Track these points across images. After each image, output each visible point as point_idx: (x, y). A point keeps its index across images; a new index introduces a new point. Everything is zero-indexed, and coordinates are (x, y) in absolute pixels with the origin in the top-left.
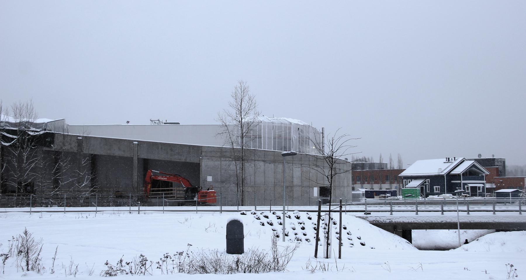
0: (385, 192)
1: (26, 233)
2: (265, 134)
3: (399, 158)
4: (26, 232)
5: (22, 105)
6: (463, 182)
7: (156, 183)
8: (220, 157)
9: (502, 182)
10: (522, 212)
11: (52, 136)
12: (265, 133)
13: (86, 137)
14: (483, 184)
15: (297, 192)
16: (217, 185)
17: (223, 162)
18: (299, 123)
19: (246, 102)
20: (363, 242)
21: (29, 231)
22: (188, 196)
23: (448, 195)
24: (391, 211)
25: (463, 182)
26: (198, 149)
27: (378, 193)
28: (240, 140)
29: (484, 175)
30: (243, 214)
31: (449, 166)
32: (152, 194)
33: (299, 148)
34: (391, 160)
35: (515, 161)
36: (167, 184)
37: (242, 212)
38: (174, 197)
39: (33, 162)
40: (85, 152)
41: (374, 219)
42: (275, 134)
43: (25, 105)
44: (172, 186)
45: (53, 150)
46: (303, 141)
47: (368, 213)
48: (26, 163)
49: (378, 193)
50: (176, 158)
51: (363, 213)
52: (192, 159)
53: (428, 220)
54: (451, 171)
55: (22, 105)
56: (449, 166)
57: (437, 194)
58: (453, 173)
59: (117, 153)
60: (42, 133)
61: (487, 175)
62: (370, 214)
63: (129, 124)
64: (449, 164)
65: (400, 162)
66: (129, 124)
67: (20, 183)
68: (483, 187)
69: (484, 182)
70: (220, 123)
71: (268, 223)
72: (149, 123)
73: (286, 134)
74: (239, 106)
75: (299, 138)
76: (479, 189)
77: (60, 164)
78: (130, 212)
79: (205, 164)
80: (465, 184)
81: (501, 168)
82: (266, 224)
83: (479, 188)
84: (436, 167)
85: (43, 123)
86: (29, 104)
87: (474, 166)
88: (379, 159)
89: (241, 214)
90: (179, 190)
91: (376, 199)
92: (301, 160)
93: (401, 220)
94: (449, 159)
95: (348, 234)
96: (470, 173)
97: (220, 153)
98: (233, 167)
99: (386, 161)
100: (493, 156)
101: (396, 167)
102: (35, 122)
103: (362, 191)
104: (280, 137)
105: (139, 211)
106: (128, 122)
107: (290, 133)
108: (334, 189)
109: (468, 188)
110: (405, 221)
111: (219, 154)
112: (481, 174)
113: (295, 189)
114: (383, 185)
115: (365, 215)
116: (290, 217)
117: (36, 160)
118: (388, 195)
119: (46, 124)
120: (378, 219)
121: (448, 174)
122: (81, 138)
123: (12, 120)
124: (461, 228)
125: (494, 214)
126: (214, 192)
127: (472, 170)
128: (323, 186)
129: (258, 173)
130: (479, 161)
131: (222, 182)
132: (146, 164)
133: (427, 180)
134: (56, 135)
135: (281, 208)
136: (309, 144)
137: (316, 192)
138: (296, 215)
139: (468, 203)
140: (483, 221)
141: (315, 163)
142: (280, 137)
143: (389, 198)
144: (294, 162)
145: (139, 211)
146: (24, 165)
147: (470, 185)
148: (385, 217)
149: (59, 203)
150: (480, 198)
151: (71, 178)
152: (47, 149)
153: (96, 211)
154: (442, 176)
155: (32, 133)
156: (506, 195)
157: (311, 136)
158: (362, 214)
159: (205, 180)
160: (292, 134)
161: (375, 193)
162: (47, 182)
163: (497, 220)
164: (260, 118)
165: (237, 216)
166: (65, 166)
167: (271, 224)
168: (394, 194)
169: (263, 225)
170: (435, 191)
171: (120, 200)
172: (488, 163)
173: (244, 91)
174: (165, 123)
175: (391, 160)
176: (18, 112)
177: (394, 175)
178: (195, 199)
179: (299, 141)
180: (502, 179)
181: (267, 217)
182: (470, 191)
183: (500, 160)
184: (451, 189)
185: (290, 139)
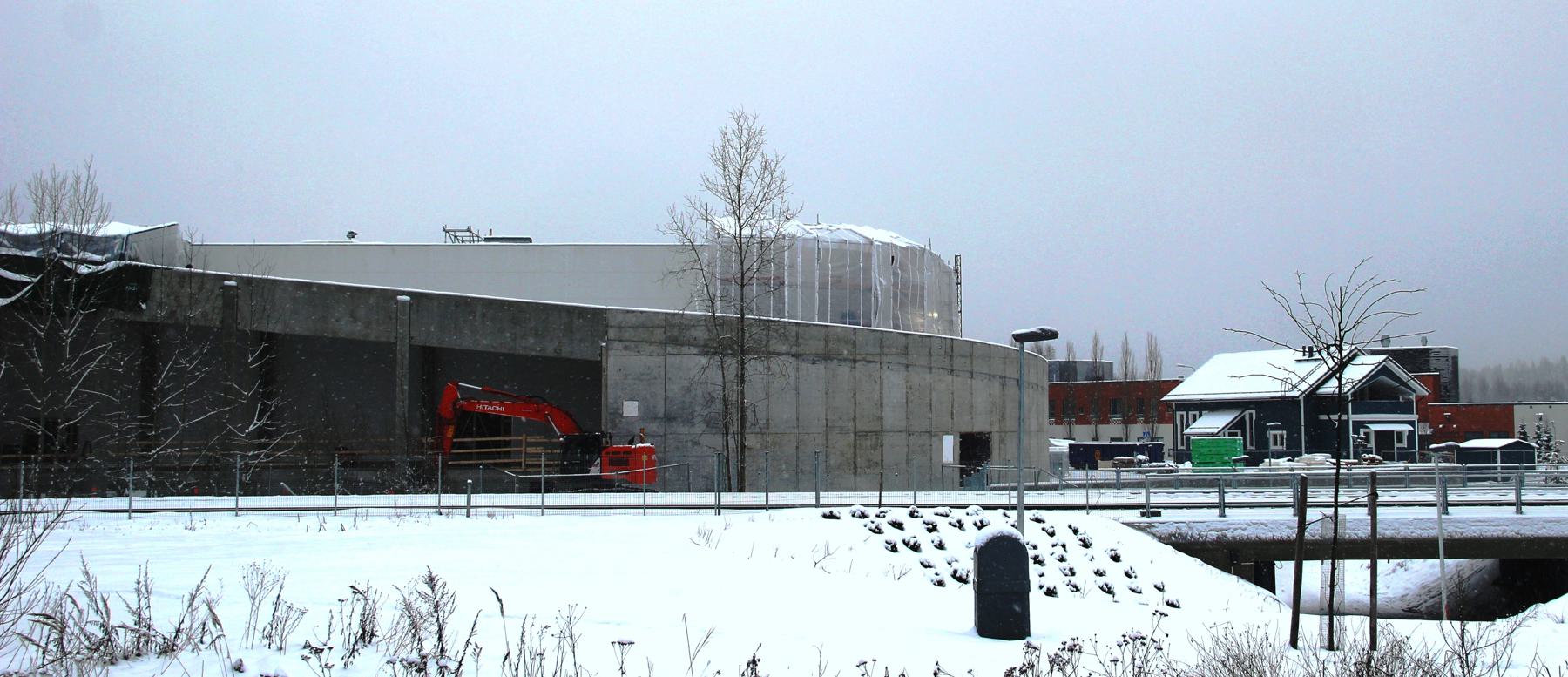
0: (1130, 450)
1: (431, 581)
2: (795, 270)
3: (1150, 346)
4: (432, 579)
5: (59, 180)
6: (1354, 417)
7: (471, 423)
8: (664, 344)
9: (1449, 421)
10: (1524, 508)
11: (143, 276)
12: (793, 274)
13: (249, 281)
14: (1412, 423)
15: (894, 449)
16: (653, 427)
17: (670, 359)
18: (895, 242)
19: (754, 178)
20: (1173, 600)
21: (440, 574)
22: (570, 463)
23: (1319, 457)
24: (1222, 506)
25: (1354, 417)
26: (595, 319)
27: (1109, 453)
28: (734, 290)
29: (1413, 397)
30: (831, 516)
31: (1312, 372)
32: (460, 457)
33: (895, 318)
34: (1127, 352)
35: (1484, 354)
36: (496, 425)
37: (827, 511)
38: (519, 464)
39: (90, 358)
40: (246, 324)
41: (1173, 529)
42: (823, 275)
43: (71, 180)
44: (508, 433)
45: (145, 319)
46: (907, 296)
47: (1150, 510)
48: (70, 361)
49: (1109, 453)
50: (530, 345)
51: (1138, 512)
52: (582, 351)
53: (1472, 532)
54: (1318, 387)
55: (59, 180)
56: (1312, 372)
57: (1279, 455)
58: (1322, 390)
59: (345, 327)
60: (111, 265)
61: (1420, 399)
62: (1159, 514)
63: (355, 241)
64: (1312, 365)
65: (1154, 358)
66: (355, 241)
67: (51, 425)
68: (1412, 433)
69: (1415, 417)
70: (674, 240)
71: (906, 544)
72: (439, 239)
73: (855, 273)
74: (733, 190)
75: (895, 285)
76: (1400, 441)
77: (176, 362)
78: (439, 509)
79: (618, 364)
80: (1358, 425)
81: (1446, 377)
82: (900, 546)
83: (1400, 434)
84: (1271, 371)
85: (115, 237)
86: (84, 179)
87: (1384, 370)
88: (1090, 346)
89: (825, 516)
90: (529, 447)
91: (1104, 473)
92: (905, 352)
93: (1251, 533)
94: (1311, 349)
95: (1127, 574)
96: (1376, 393)
97: (670, 333)
98: (715, 375)
99: (1112, 356)
100: (1425, 341)
101: (1141, 372)
102: (100, 233)
103: (1061, 445)
104: (839, 281)
105: (469, 507)
106: (352, 235)
107: (868, 270)
108: (1002, 441)
109: (1367, 434)
110: (1263, 536)
111: (659, 334)
112: (1403, 393)
113: (887, 440)
114: (1102, 428)
115: (1145, 519)
116: (960, 525)
117: (103, 350)
118: (1140, 457)
119: (126, 239)
120: (1184, 530)
121: (1312, 395)
122: (233, 283)
123: (27, 229)
124: (1450, 554)
125: (1519, 512)
126: (649, 451)
127: (1382, 384)
128: (969, 430)
129: (782, 393)
130: (1403, 356)
131: (669, 418)
132: (430, 361)
133: (1247, 413)
134: (157, 276)
135: (873, 497)
136: (922, 306)
137: (949, 448)
138: (977, 519)
139: (1219, 484)
140: (1489, 534)
141: (946, 364)
142: (839, 281)
143: (1146, 466)
144: (885, 359)
145: (469, 507)
146: (64, 367)
147: (1375, 427)
148: (1204, 521)
149: (174, 485)
150: (1402, 465)
151: (213, 405)
152: (129, 317)
153: (335, 509)
154: (1294, 400)
155: (83, 269)
156: (1487, 455)
157: (928, 277)
158: (1134, 516)
159: (618, 412)
160: (875, 274)
161: (1098, 453)
162: (134, 420)
163: (1527, 532)
164: (791, 228)
165: (999, 524)
166: (195, 368)
167: (916, 548)
168: (1156, 454)
169: (894, 549)
170: (1272, 447)
171: (362, 477)
172: (1415, 359)
173: (749, 141)
174: (487, 240)
175: (1127, 352)
176: (47, 197)
177: (1147, 399)
178: (594, 471)
179: (895, 295)
180: (1450, 408)
181: (898, 525)
182: (1372, 444)
183: (1443, 353)
184: (1330, 439)
185: (868, 289)
